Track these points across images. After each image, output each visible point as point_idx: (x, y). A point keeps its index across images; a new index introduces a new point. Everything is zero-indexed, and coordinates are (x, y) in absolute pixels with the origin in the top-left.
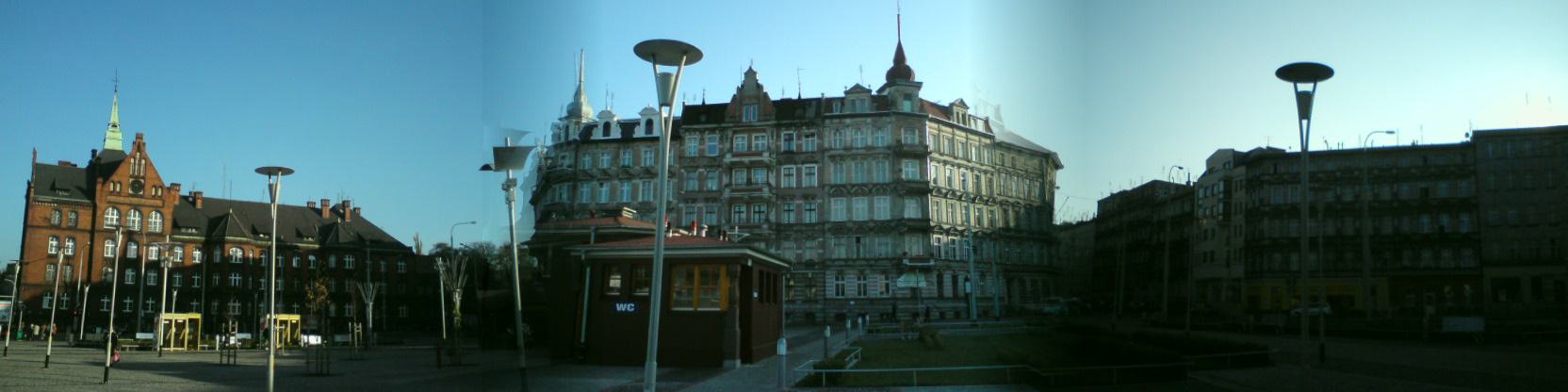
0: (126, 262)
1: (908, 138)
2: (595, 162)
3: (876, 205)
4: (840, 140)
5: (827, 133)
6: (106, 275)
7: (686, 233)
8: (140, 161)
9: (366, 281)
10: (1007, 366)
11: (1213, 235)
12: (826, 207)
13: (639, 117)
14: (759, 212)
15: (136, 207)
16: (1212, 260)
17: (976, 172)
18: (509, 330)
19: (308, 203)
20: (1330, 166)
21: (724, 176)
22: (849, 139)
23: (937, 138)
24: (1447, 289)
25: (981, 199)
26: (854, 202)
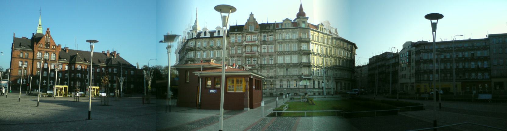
1: (303, 36)
3: (293, 58)
4: (281, 37)
5: (276, 34)
6: (37, 73)
8: (48, 37)
11: (405, 69)
13: (215, 30)
14: (255, 60)
15: (47, 52)
16: (405, 77)
20: (442, 47)
22: (284, 36)
24: (480, 85)
25: (328, 56)
26: (286, 58)
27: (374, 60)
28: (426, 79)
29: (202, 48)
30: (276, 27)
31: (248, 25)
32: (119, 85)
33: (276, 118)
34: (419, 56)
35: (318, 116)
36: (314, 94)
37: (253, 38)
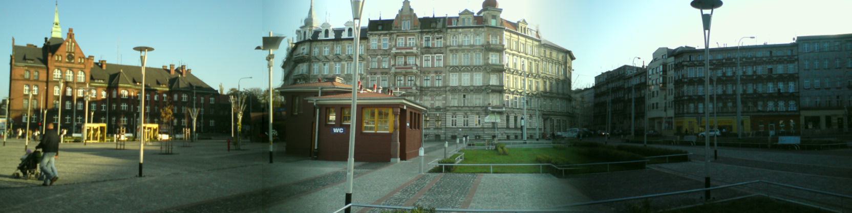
0: (65, 98)
1: (493, 41)
2: (320, 52)
3: (475, 77)
4: (456, 41)
7: (371, 91)
8: (71, 44)
9: (193, 107)
10: (541, 164)
11: (657, 94)
12: (447, 78)
14: (411, 80)
15: (70, 69)
16: (657, 108)
17: (530, 61)
18: (266, 133)
19: (163, 67)
20: (720, 57)
21: (391, 60)
22: (460, 40)
23: (509, 40)
24: (781, 122)
27: (605, 80)
28: (692, 110)
29: (321, 57)
30: (448, 25)
31: (401, 20)
32: (191, 121)
33: (443, 174)
34: (680, 73)
35: (512, 173)
36: (508, 137)
37: (408, 42)
